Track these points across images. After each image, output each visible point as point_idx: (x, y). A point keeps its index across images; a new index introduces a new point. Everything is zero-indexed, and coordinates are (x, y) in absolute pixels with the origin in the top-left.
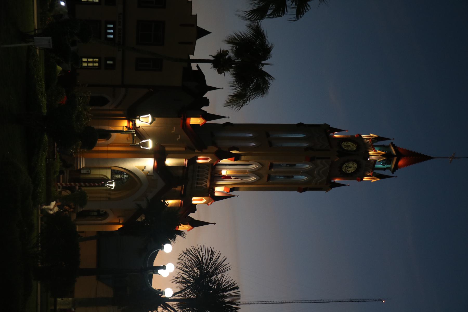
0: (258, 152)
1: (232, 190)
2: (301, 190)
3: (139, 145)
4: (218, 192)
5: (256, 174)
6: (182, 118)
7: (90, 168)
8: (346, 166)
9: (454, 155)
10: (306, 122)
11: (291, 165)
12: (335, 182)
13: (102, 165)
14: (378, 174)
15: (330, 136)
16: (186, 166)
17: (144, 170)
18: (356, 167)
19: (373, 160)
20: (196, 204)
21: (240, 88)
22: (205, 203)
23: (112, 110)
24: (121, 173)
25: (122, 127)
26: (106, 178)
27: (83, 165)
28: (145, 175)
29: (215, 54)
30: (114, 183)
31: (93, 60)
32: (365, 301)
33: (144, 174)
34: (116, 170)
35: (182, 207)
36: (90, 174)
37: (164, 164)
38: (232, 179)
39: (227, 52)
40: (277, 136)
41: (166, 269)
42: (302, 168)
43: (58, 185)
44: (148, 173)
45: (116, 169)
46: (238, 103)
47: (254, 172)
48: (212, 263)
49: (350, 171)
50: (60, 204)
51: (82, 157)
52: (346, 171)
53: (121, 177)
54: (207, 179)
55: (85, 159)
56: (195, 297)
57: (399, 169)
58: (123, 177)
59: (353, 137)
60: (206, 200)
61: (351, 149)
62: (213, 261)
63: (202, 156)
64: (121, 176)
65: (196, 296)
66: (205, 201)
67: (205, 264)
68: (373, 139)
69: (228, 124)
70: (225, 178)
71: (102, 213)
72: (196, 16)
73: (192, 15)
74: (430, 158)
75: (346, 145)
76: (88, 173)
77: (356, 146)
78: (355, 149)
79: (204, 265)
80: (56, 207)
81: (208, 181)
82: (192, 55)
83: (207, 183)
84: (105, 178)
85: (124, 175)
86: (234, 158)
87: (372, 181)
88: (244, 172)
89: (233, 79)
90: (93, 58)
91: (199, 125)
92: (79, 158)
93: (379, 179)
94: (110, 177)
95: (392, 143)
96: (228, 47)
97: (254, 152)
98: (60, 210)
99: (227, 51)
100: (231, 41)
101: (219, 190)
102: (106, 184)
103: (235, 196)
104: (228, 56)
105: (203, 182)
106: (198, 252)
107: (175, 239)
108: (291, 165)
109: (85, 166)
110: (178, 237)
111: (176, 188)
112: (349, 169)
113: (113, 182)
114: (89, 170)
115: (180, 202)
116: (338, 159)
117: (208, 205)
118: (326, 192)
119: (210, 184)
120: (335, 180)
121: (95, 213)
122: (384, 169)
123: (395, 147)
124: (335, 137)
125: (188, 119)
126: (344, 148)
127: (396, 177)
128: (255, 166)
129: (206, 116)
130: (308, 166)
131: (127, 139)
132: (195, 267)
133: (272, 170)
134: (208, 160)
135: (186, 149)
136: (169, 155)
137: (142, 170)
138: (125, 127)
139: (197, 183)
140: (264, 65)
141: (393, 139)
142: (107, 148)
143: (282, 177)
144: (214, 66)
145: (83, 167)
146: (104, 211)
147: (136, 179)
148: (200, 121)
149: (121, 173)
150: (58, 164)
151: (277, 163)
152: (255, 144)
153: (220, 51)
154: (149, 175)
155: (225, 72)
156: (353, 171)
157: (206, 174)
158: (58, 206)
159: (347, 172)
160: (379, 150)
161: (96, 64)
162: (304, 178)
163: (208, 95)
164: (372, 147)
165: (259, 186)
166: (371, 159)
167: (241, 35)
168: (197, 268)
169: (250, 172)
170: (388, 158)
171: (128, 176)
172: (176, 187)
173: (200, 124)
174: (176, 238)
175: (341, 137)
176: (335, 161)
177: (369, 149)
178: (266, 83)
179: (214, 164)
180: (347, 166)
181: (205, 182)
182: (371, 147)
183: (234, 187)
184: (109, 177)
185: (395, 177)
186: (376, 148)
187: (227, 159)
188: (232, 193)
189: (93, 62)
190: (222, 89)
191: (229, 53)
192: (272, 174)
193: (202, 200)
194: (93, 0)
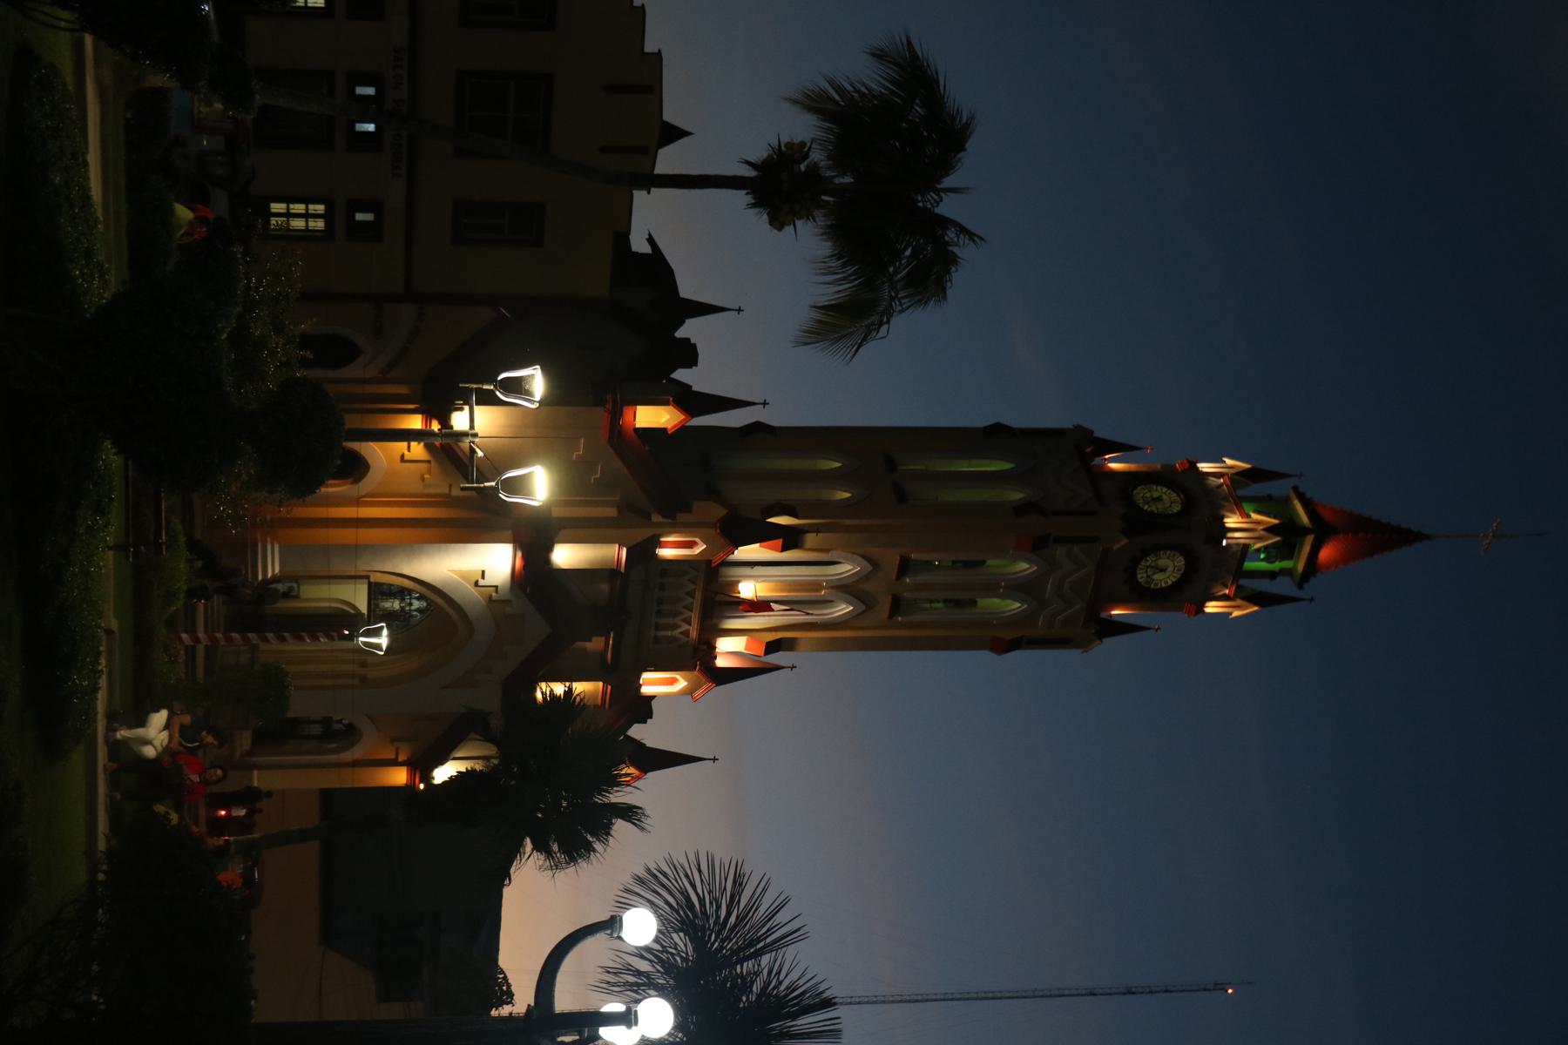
0: (864, 522)
3: (495, 489)
6: (609, 406)
7: (297, 579)
8: (1150, 566)
10: (1017, 419)
11: (968, 565)
12: (1113, 618)
13: (338, 566)
16: (623, 570)
17: (481, 582)
19: (1238, 544)
20: (653, 697)
21: (856, 279)
23: (365, 381)
26: (352, 611)
29: (759, 153)
31: (307, 209)
33: (477, 594)
34: (384, 584)
35: (607, 706)
36: (297, 597)
37: (548, 561)
38: (773, 610)
39: (806, 149)
40: (923, 467)
41: (636, 1024)
44: (494, 594)
45: (383, 581)
47: (845, 589)
49: (1161, 581)
50: (187, 719)
51: (269, 539)
52: (1147, 582)
54: (692, 611)
55: (280, 547)
56: (678, 1040)
57: (1319, 574)
59: (1168, 469)
60: (686, 683)
67: (712, 921)
68: (1235, 477)
69: (757, 428)
71: (337, 726)
75: (1148, 495)
78: (1177, 508)
79: (709, 925)
81: (695, 617)
82: (646, 192)
85: (410, 599)
86: (779, 542)
88: (814, 586)
89: (824, 248)
90: (307, 201)
91: (664, 430)
92: (260, 545)
93: (1256, 608)
95: (1296, 489)
96: (802, 128)
97: (848, 522)
99: (803, 144)
100: (815, 103)
101: (729, 649)
102: (358, 637)
103: (783, 668)
104: (806, 163)
105: (677, 620)
106: (687, 876)
107: (608, 834)
108: (968, 565)
109: (280, 571)
110: (620, 827)
112: (1158, 577)
114: (295, 585)
116: (1125, 541)
118: (1082, 653)
119: (701, 631)
120: (1113, 612)
121: (316, 729)
122: (1272, 575)
123: (1307, 504)
125: (627, 411)
126: (1141, 505)
127: (1312, 600)
129: (689, 401)
130: (1024, 566)
131: (423, 479)
132: (676, 932)
133: (908, 580)
134: (695, 548)
135: (620, 511)
136: (563, 533)
139: (657, 627)
141: (1301, 476)
142: (355, 509)
143: (938, 602)
145: (273, 576)
146: (345, 722)
147: (452, 613)
149: (401, 593)
150: (180, 569)
151: (925, 557)
153: (777, 143)
154: (495, 601)
155: (799, 223)
156: (1170, 582)
159: (1152, 586)
160: (1254, 512)
163: (690, 329)
165: (869, 634)
166: (1230, 541)
167: (849, 88)
168: (682, 934)
169: (832, 587)
170: (1287, 536)
171: (425, 604)
172: (586, 641)
173: (669, 427)
174: (612, 832)
177: (1223, 507)
178: (949, 260)
179: (716, 560)
180: (1153, 564)
183: (781, 639)
186: (1247, 507)
187: (758, 544)
188: (774, 659)
189: (307, 216)
190: (739, 310)
191: (811, 153)
192: (905, 594)
193: (672, 681)
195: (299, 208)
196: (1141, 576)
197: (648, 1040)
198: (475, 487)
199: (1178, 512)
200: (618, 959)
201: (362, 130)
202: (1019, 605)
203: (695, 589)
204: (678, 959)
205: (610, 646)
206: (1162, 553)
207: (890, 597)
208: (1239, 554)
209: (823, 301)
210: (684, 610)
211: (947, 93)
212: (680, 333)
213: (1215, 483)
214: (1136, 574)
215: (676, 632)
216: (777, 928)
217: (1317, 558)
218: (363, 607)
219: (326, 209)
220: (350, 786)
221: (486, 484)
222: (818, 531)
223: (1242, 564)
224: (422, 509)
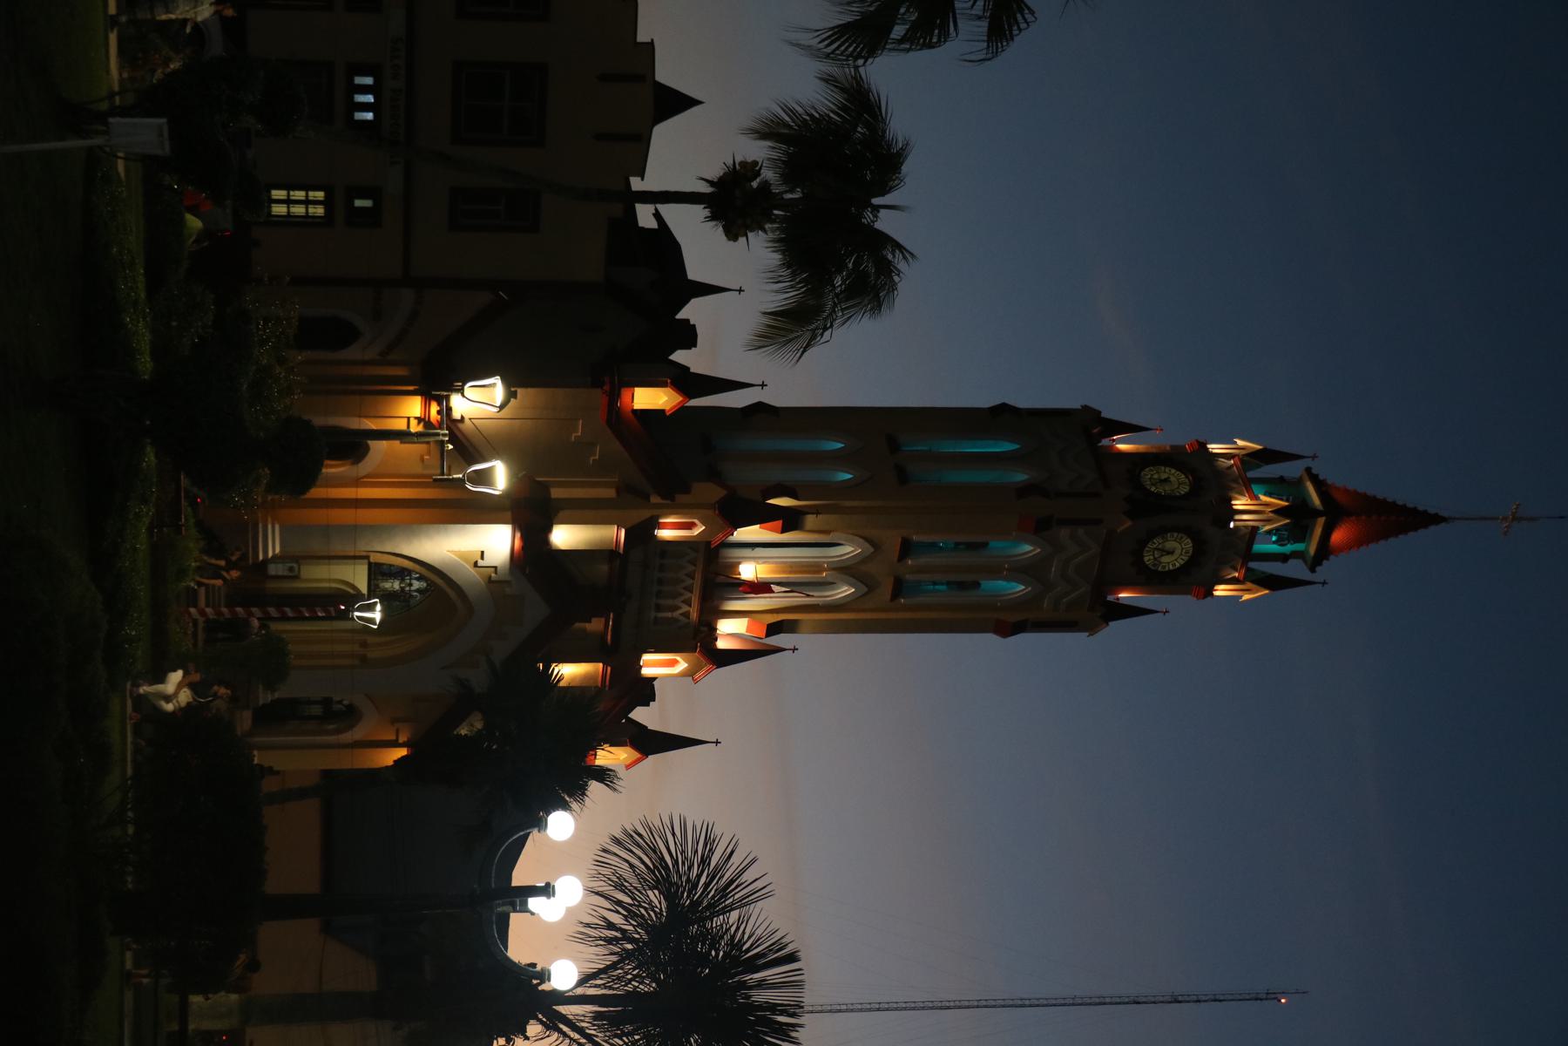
0: (864, 503)
1: (773, 629)
2: (1006, 629)
3: (462, 481)
4: (729, 638)
6: (606, 387)
8: (1156, 549)
10: (1022, 401)
12: (1120, 602)
14: (1263, 573)
16: (621, 551)
17: (481, 563)
19: (1246, 527)
20: (654, 679)
21: (802, 287)
22: (684, 674)
23: (365, 363)
25: (406, 420)
26: (352, 591)
27: (274, 547)
28: (483, 583)
29: (715, 172)
30: (378, 607)
31: (307, 196)
32: (1222, 998)
33: (478, 576)
36: (296, 577)
37: (547, 542)
38: (773, 592)
39: (757, 168)
41: (554, 896)
43: (189, 614)
44: (493, 575)
46: (793, 339)
47: (846, 570)
49: (1169, 563)
50: (196, 677)
51: (269, 519)
53: (402, 589)
54: (692, 592)
55: (280, 527)
57: (1332, 557)
58: (407, 589)
60: (686, 665)
61: (1173, 490)
64: (400, 583)
65: (654, 985)
67: (684, 879)
69: (760, 407)
70: (749, 590)
71: (337, 707)
72: (650, 46)
74: (1437, 519)
76: (291, 574)
78: (1184, 490)
79: (682, 882)
80: (185, 689)
82: (639, 179)
85: (410, 579)
86: (779, 523)
87: (1244, 598)
88: (816, 568)
89: (775, 258)
90: (307, 188)
91: (663, 411)
92: (260, 525)
93: (1267, 592)
95: (1308, 470)
96: (758, 151)
99: (755, 163)
100: (769, 131)
101: (730, 631)
102: (353, 612)
104: (758, 180)
105: (678, 602)
107: (584, 794)
109: (281, 551)
110: (595, 787)
111: (587, 625)
112: (1166, 559)
114: (295, 565)
116: (1129, 523)
117: (696, 681)
119: (701, 612)
120: (1120, 595)
121: (317, 710)
122: (1284, 558)
123: (1319, 484)
124: (1117, 449)
125: (625, 393)
127: (1324, 583)
129: (687, 382)
130: (1027, 548)
131: (422, 460)
133: (910, 562)
135: (618, 493)
137: (473, 562)
138: (416, 421)
139: (658, 608)
141: (1314, 457)
142: (354, 490)
143: (942, 584)
144: (711, 212)
145: (274, 556)
146: (345, 702)
147: (452, 594)
149: (401, 573)
152: (850, 476)
153: (732, 162)
155: (750, 235)
156: (1178, 565)
157: (686, 575)
158: (192, 686)
159: (1160, 569)
161: (314, 210)
163: (692, 311)
168: (656, 892)
169: (834, 569)
170: (1297, 518)
171: (425, 585)
172: (585, 622)
174: (588, 793)
176: (1119, 531)
177: (1232, 489)
179: (716, 541)
180: (1160, 546)
183: (782, 621)
185: (1320, 585)
186: (1256, 488)
187: (758, 526)
188: (776, 640)
189: (307, 202)
190: (740, 291)
191: (762, 171)
192: (907, 576)
193: (673, 663)
195: (299, 195)
196: (1148, 559)
197: (571, 908)
198: (445, 479)
199: (1186, 494)
200: (594, 913)
201: (361, 83)
202: (1023, 587)
203: (694, 571)
204: (652, 913)
205: (610, 628)
206: (1169, 535)
207: (892, 579)
208: (1247, 537)
209: (771, 307)
210: (682, 591)
211: (889, 115)
212: (682, 315)
213: (1225, 465)
214: (1143, 556)
215: (676, 614)
216: (743, 886)
217: (1329, 541)
218: (363, 587)
219: (326, 197)
220: (350, 767)
221: (455, 476)
222: (817, 513)
223: (1252, 547)
224: (429, 490)
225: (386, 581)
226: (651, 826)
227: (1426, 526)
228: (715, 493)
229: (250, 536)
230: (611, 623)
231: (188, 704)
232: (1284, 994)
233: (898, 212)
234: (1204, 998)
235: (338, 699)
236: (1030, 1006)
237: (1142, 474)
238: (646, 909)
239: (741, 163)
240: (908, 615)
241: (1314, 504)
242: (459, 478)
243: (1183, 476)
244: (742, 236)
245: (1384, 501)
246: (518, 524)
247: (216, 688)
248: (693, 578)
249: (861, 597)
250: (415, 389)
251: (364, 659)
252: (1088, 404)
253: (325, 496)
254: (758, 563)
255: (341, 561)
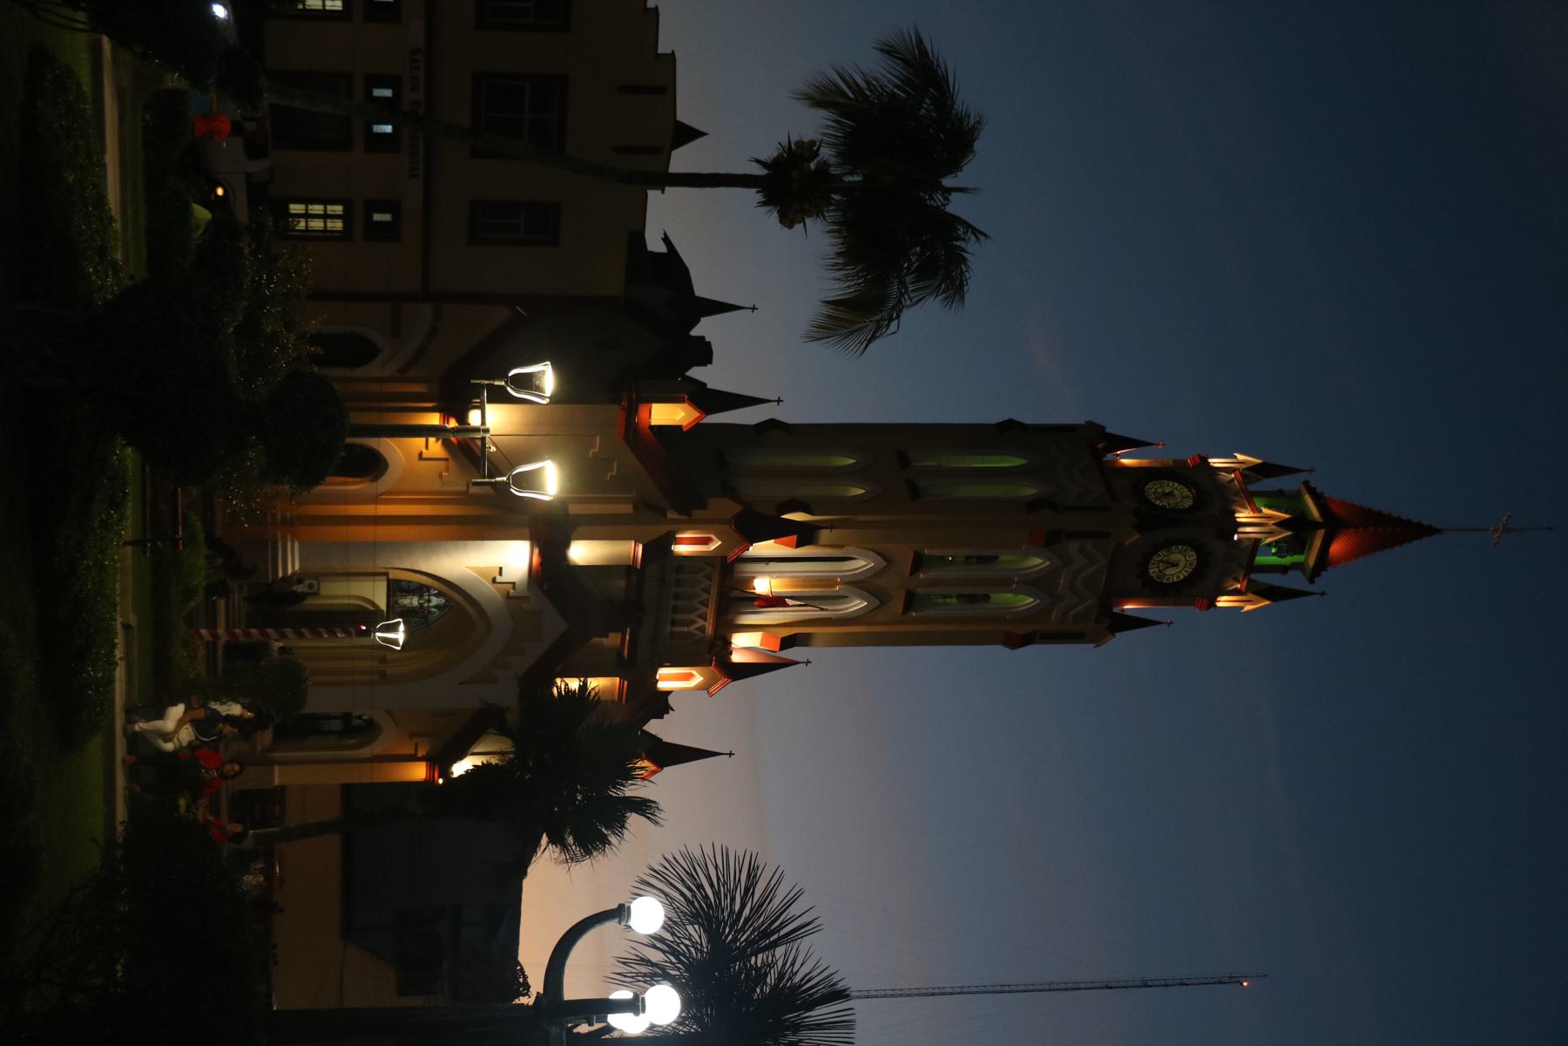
1: (787, 643)
2: (1016, 641)
3: (506, 484)
5: (868, 592)
8: (1162, 561)
9: (1507, 520)
14: (1264, 584)
15: (1107, 461)
16: (639, 566)
17: (499, 579)
18: (1195, 564)
19: (1249, 539)
20: (668, 693)
22: (699, 688)
23: (381, 380)
24: (422, 589)
26: (371, 608)
28: (500, 597)
29: (769, 152)
30: (402, 628)
32: (1188, 982)
36: (316, 594)
37: (565, 558)
38: (788, 606)
40: (934, 464)
41: (644, 1011)
42: (1023, 569)
43: (201, 637)
44: (511, 591)
46: (856, 330)
47: (859, 584)
48: (752, 909)
51: (289, 537)
53: (421, 605)
56: (692, 1030)
57: (1330, 569)
58: (426, 605)
59: (1180, 464)
60: (702, 679)
61: (1177, 504)
62: (755, 900)
63: (690, 531)
66: (698, 678)
68: (1247, 472)
69: (772, 424)
70: (764, 604)
71: (357, 722)
72: (671, 57)
73: (658, 55)
74: (1430, 531)
75: (1160, 490)
76: (310, 591)
77: (1192, 493)
78: (1188, 503)
79: (724, 917)
80: (188, 726)
81: (710, 613)
82: (660, 192)
83: (706, 620)
84: (366, 609)
85: (429, 595)
86: (794, 537)
88: (829, 582)
90: (325, 202)
91: (680, 427)
93: (1268, 602)
94: (383, 605)
95: (1306, 484)
97: (862, 518)
98: (200, 737)
99: (812, 143)
101: (745, 644)
102: (374, 633)
103: (797, 663)
104: (815, 161)
105: (693, 616)
107: (623, 827)
109: (300, 568)
110: (634, 820)
111: (604, 640)
112: (1171, 571)
113: (399, 623)
114: (315, 582)
115: (618, 684)
116: (1138, 536)
117: (711, 695)
119: (717, 626)
122: (1283, 569)
123: (1318, 498)
124: (1122, 464)
125: (643, 409)
126: (1153, 500)
127: (1323, 594)
128: (864, 563)
131: (441, 476)
135: (635, 508)
136: (581, 529)
137: (491, 578)
139: (674, 623)
140: (953, 194)
141: (1311, 471)
143: (952, 597)
146: (365, 717)
147: (471, 610)
148: (683, 414)
149: (420, 590)
150: (199, 566)
151: (937, 552)
154: (514, 597)
155: (808, 221)
156: (1182, 577)
157: (702, 590)
158: (196, 724)
161: (333, 225)
162: (1025, 600)
163: (705, 328)
164: (1242, 495)
167: (862, 84)
168: (696, 926)
169: (847, 583)
170: (1298, 530)
171: (443, 601)
172: (601, 637)
174: (627, 825)
175: (1143, 465)
176: (1127, 543)
177: (1234, 502)
179: (732, 556)
180: (1165, 559)
181: (699, 616)
182: (1241, 497)
183: (795, 635)
184: (382, 604)
186: (1258, 502)
187: (773, 541)
188: (789, 654)
190: (754, 309)
191: (822, 149)
192: (919, 590)
193: (688, 677)
194: (324, 5)
199: (1190, 507)
202: (1032, 600)
204: (692, 950)
206: (1173, 548)
209: (832, 296)
210: (698, 606)
212: (695, 332)
221: (498, 479)
222: (832, 527)
225: (405, 597)
226: (692, 857)
227: (1431, 535)
228: (731, 508)
229: (270, 554)
230: (627, 638)
231: (190, 742)
232: (1246, 977)
233: (967, 195)
234: (1171, 982)
235: (358, 714)
236: (1010, 992)
237: (1147, 487)
238: (686, 946)
239: (797, 143)
240: (920, 628)
241: (1313, 515)
242: (503, 482)
243: (1186, 490)
244: (800, 222)
245: (1380, 514)
246: (536, 540)
247: (221, 725)
248: (709, 593)
249: (875, 609)
250: (435, 406)
251: (383, 675)
252: (1093, 420)
253: (343, 514)
254: (772, 578)
255: (358, 578)
